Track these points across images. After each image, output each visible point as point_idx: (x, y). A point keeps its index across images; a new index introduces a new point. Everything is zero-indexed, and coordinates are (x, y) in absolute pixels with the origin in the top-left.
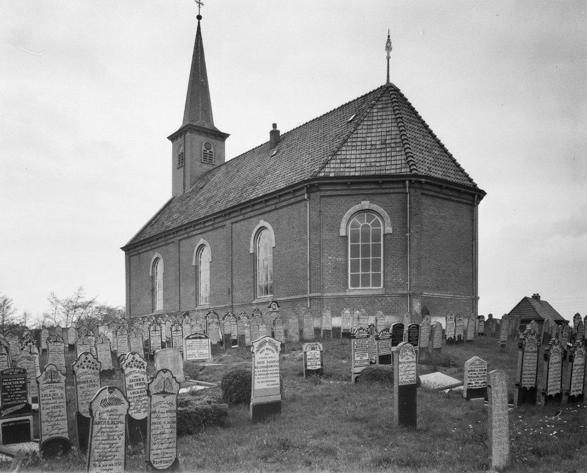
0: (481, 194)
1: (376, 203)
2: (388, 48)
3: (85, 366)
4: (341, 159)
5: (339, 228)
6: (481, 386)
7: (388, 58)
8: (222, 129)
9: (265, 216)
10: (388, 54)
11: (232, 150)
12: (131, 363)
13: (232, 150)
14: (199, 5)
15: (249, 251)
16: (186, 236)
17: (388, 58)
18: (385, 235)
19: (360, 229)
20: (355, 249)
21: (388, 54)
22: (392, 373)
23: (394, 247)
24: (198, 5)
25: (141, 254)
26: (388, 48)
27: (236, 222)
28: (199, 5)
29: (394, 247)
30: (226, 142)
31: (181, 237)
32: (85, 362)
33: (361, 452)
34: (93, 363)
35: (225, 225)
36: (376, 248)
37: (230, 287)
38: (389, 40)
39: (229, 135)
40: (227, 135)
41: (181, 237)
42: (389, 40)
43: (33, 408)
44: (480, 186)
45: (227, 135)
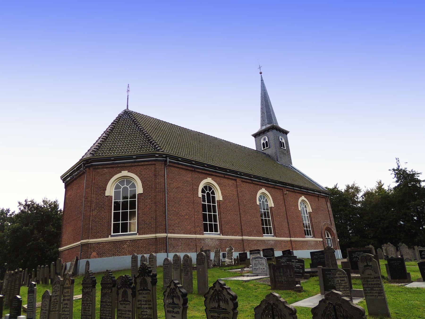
19: (121, 190)
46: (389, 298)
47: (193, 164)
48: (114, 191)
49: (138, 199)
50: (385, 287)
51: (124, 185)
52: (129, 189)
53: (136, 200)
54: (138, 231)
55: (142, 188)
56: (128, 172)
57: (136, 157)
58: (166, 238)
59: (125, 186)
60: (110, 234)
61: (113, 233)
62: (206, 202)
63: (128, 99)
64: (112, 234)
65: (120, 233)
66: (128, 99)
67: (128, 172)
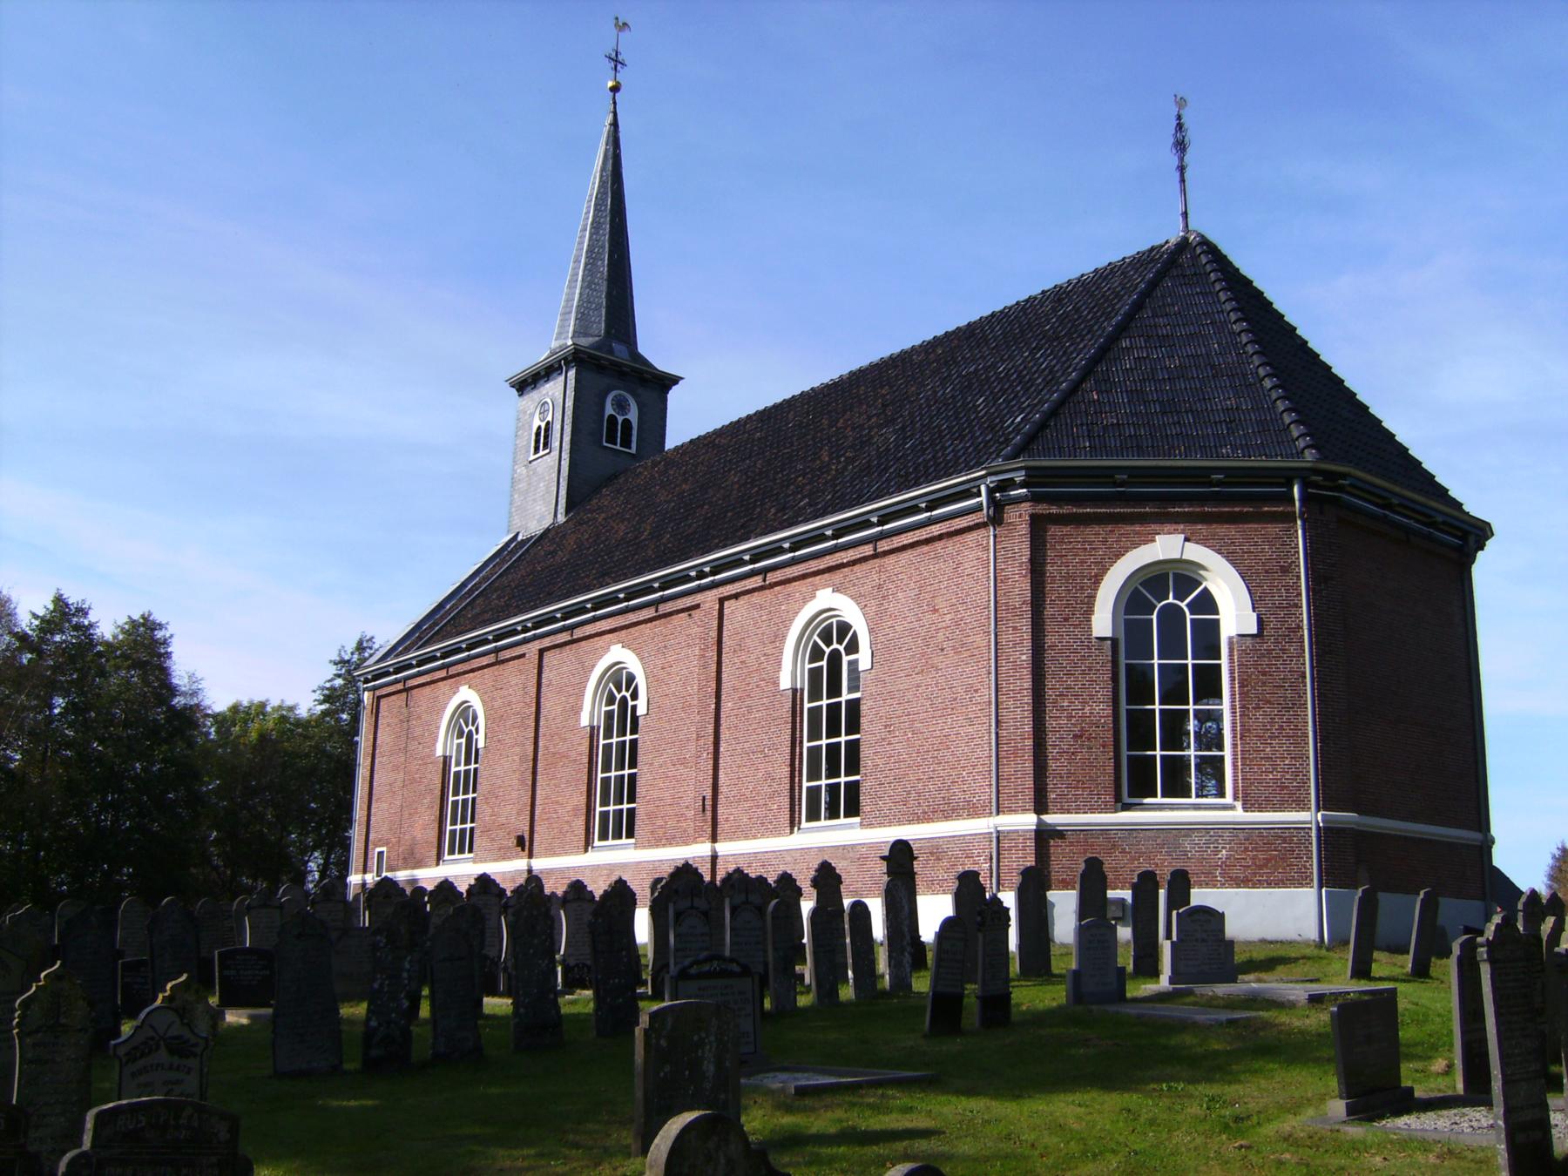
0: (1476, 534)
1: (1203, 542)
2: (1181, 146)
4: (1075, 413)
5: (1090, 611)
7: (1182, 169)
9: (837, 577)
10: (1181, 159)
14: (616, 66)
15: (776, 683)
16: (564, 637)
17: (1182, 169)
21: (1181, 159)
22: (345, 771)
23: (1264, 674)
24: (613, 64)
25: (414, 692)
26: (1181, 146)
27: (736, 596)
28: (616, 66)
29: (1264, 674)
30: (669, 396)
31: (547, 642)
35: (697, 606)
37: (708, 793)
39: (682, 378)
40: (675, 380)
41: (547, 642)
44: (1475, 506)
45: (675, 380)
52: (1189, 617)
54: (1236, 798)
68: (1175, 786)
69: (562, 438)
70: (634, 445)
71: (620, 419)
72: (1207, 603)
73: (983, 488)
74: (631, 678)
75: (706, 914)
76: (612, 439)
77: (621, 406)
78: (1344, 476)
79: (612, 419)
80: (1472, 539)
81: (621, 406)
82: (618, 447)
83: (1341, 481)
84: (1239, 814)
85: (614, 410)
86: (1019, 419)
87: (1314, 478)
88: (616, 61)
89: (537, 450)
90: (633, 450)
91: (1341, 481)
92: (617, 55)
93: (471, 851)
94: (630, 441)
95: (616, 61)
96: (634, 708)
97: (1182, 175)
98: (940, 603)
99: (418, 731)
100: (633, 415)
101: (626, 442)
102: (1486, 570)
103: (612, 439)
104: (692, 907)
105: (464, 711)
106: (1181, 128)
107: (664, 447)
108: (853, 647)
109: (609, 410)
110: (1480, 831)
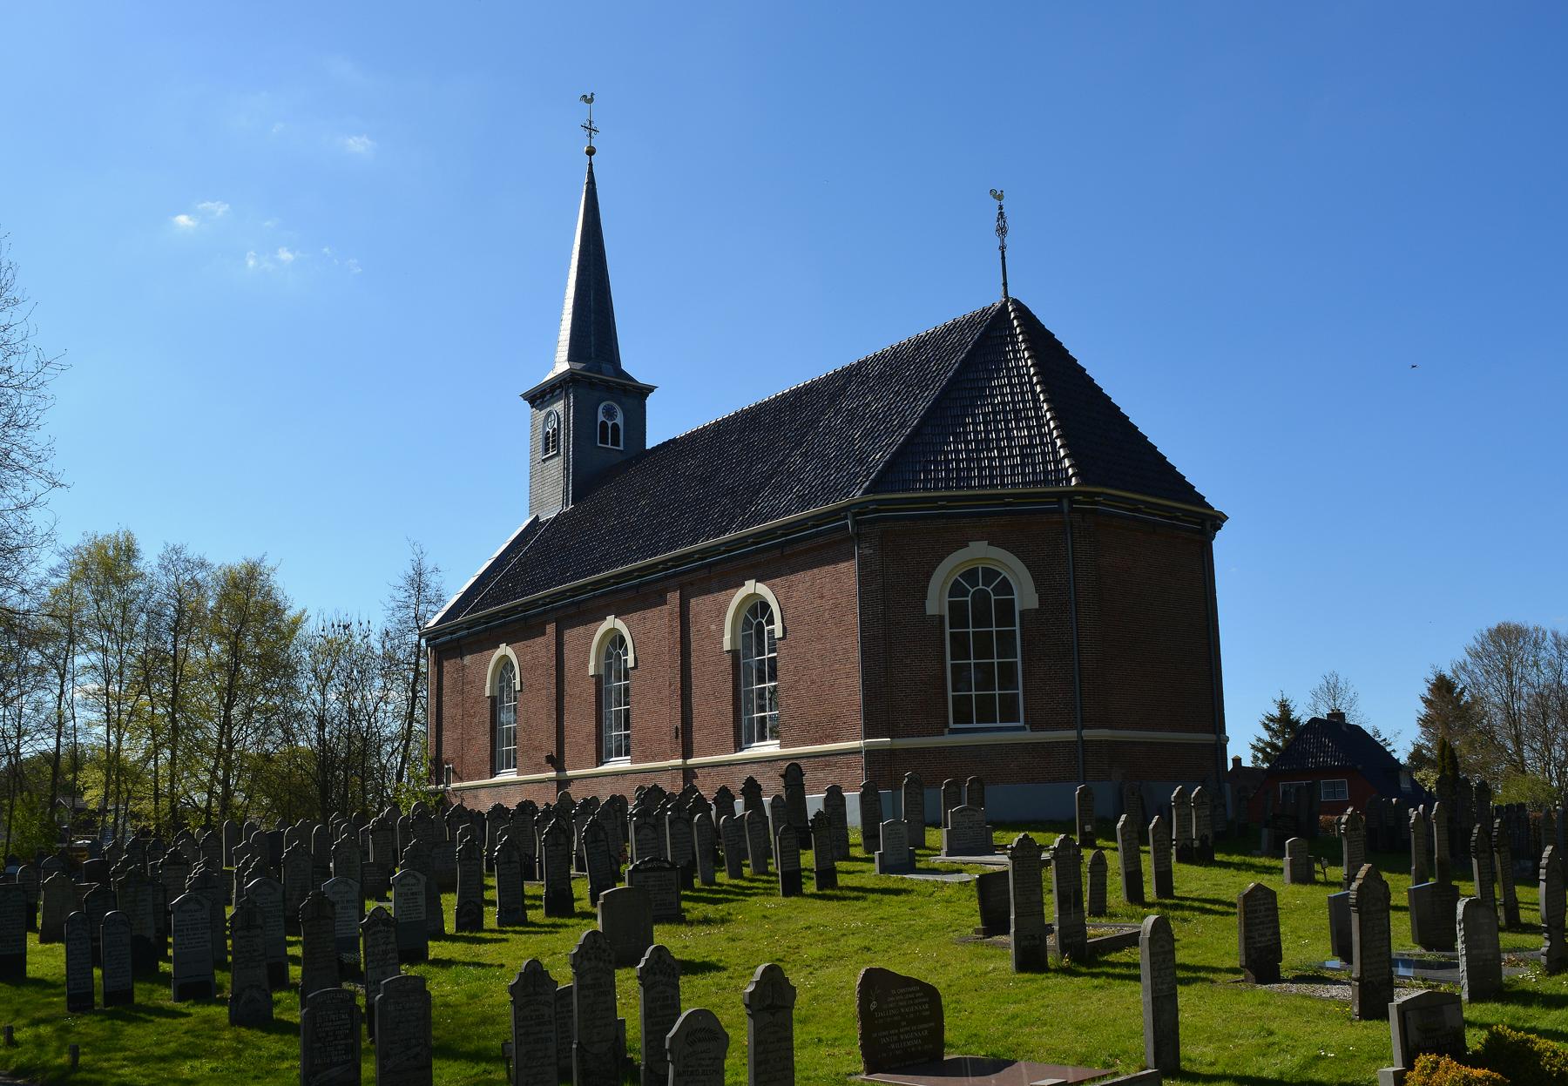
0: (1216, 520)
2: (1002, 231)
3: (593, 956)
6: (1270, 940)
7: (1003, 248)
8: (642, 378)
10: (1003, 241)
11: (662, 425)
12: (590, 951)
13: (662, 425)
17: (1003, 248)
18: (1022, 613)
19: (969, 599)
20: (959, 642)
21: (1003, 241)
26: (1002, 231)
32: (592, 948)
33: (270, 591)
34: (604, 951)
36: (1006, 640)
38: (1001, 214)
40: (651, 389)
42: (1001, 214)
43: (620, 974)
44: (1216, 501)
45: (651, 389)
46: (1391, 915)
47: (1177, 518)
48: (949, 602)
49: (943, 632)
50: (1236, 879)
51: (970, 591)
52: (993, 598)
53: (1015, 631)
54: (1026, 722)
55: (1037, 595)
56: (989, 544)
57: (867, 507)
58: (1216, 744)
59: (989, 590)
60: (946, 724)
61: (954, 723)
62: (771, 655)
63: (1003, 258)
64: (952, 726)
65: (998, 724)
66: (1003, 258)
67: (989, 544)
68: (986, 715)
69: (566, 441)
70: (622, 443)
71: (610, 424)
72: (1005, 587)
73: (849, 514)
74: (622, 639)
75: (653, 826)
76: (604, 440)
77: (610, 413)
78: (1099, 494)
79: (603, 423)
80: (1208, 525)
81: (610, 413)
82: (609, 446)
83: (1096, 499)
84: (1028, 736)
85: (605, 417)
86: (878, 457)
87: (1076, 498)
88: (590, 129)
89: (547, 451)
90: (621, 448)
91: (1096, 499)
92: (590, 124)
93: (514, 767)
94: (619, 442)
95: (590, 129)
96: (626, 661)
97: (1003, 252)
98: (826, 592)
99: (470, 678)
100: (619, 420)
101: (616, 442)
102: (1221, 544)
103: (604, 440)
104: (645, 823)
105: (505, 663)
106: (1002, 217)
107: (645, 446)
108: (771, 621)
109: (601, 418)
110: (1215, 733)
